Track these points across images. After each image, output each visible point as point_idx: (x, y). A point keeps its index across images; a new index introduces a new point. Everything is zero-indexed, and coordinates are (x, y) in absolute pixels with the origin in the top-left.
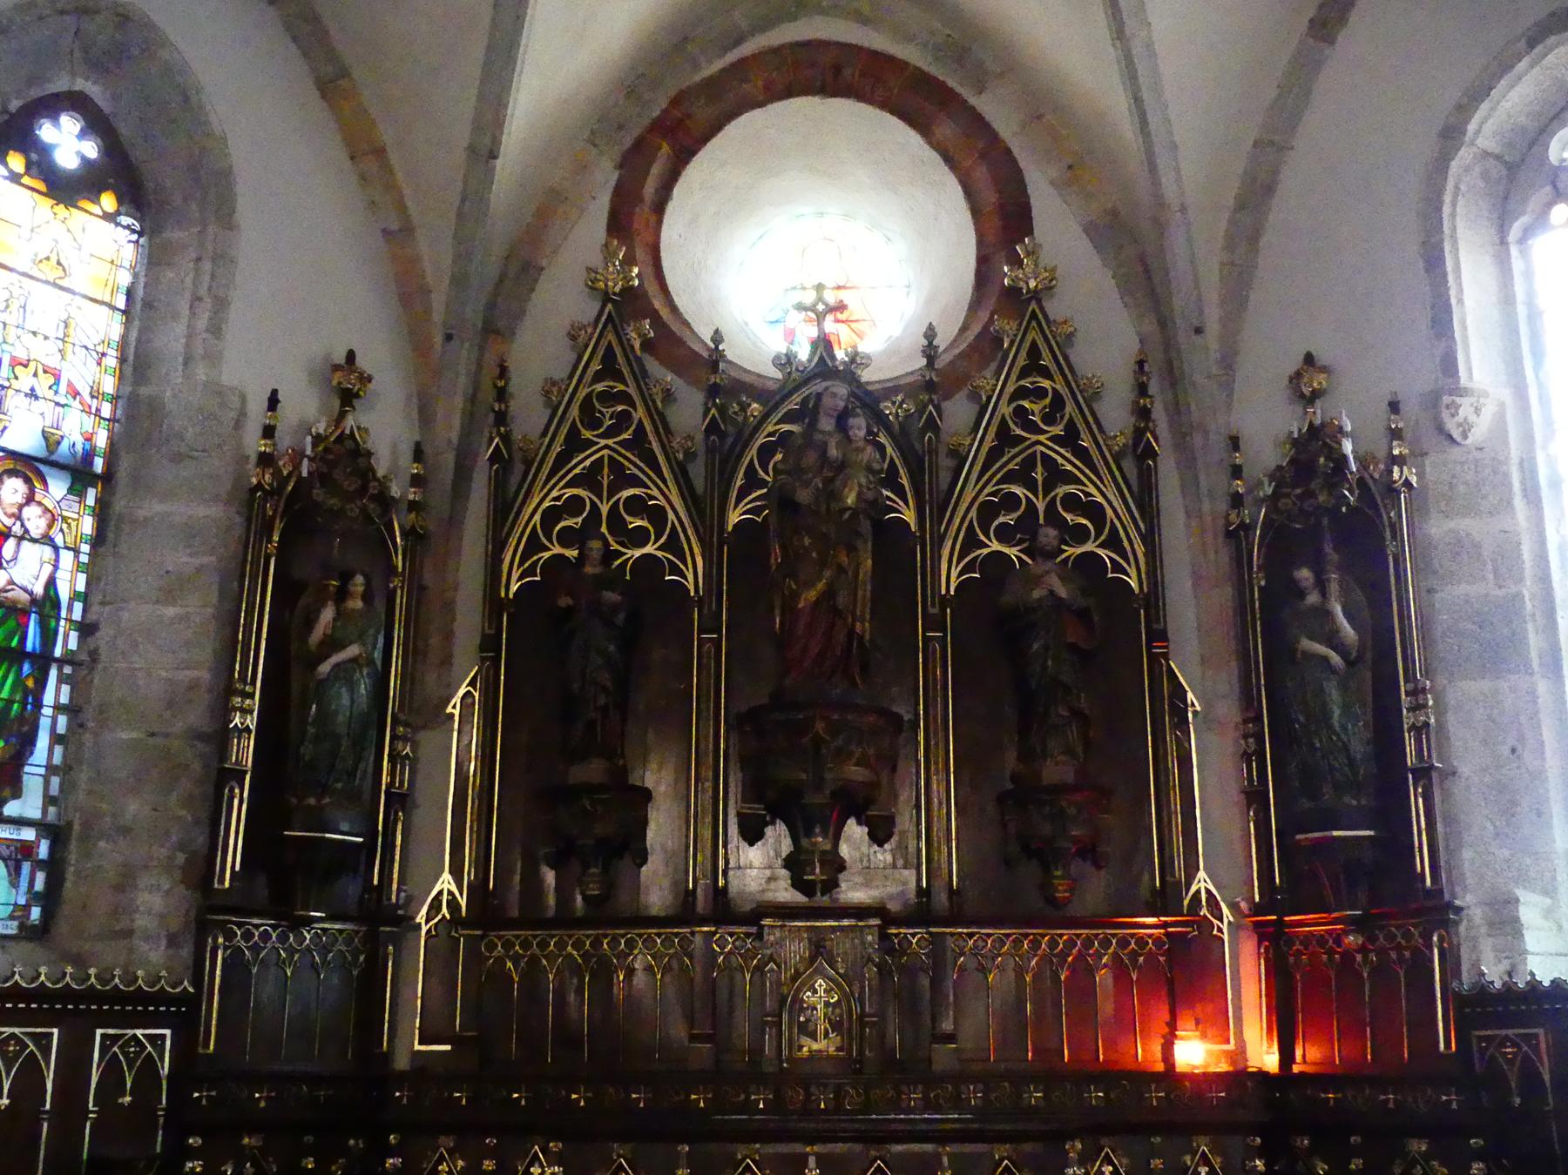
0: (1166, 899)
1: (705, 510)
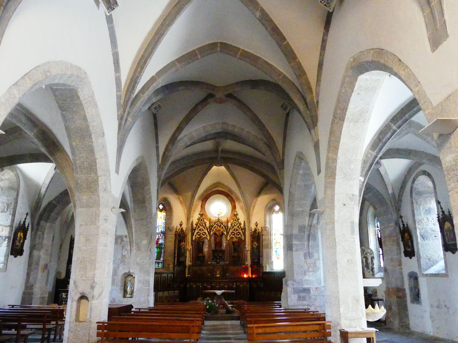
0: (244, 264)
1: (209, 233)
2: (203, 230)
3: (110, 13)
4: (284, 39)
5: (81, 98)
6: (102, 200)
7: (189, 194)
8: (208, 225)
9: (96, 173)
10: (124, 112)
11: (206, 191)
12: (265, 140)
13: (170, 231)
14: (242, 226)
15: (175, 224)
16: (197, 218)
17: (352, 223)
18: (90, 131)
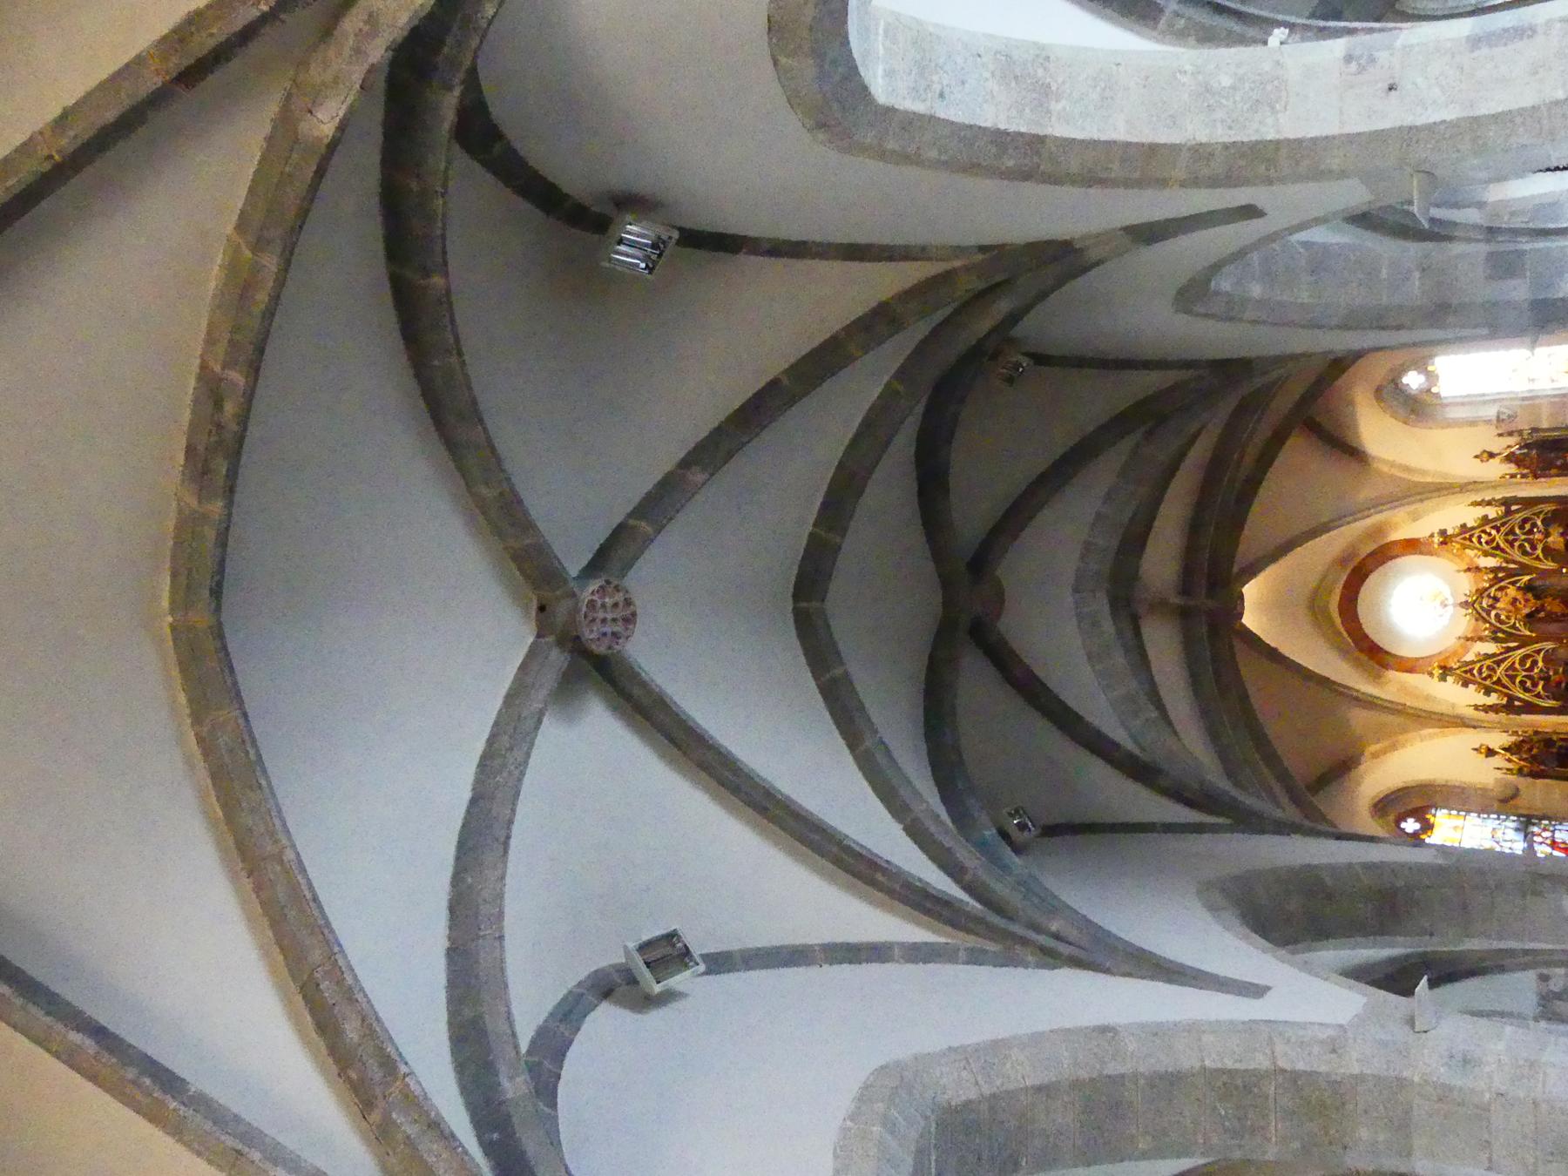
2: (1512, 667)
3: (698, 960)
4: (774, 384)
5: (972, 1094)
6: (1376, 1067)
7: (1359, 718)
8: (1491, 648)
9: (1258, 1076)
10: (1024, 942)
11: (1344, 652)
12: (1138, 435)
13: (1516, 794)
14: (1492, 512)
15: (1488, 774)
16: (1458, 688)
17: (1475, 42)
18: (1092, 1080)
